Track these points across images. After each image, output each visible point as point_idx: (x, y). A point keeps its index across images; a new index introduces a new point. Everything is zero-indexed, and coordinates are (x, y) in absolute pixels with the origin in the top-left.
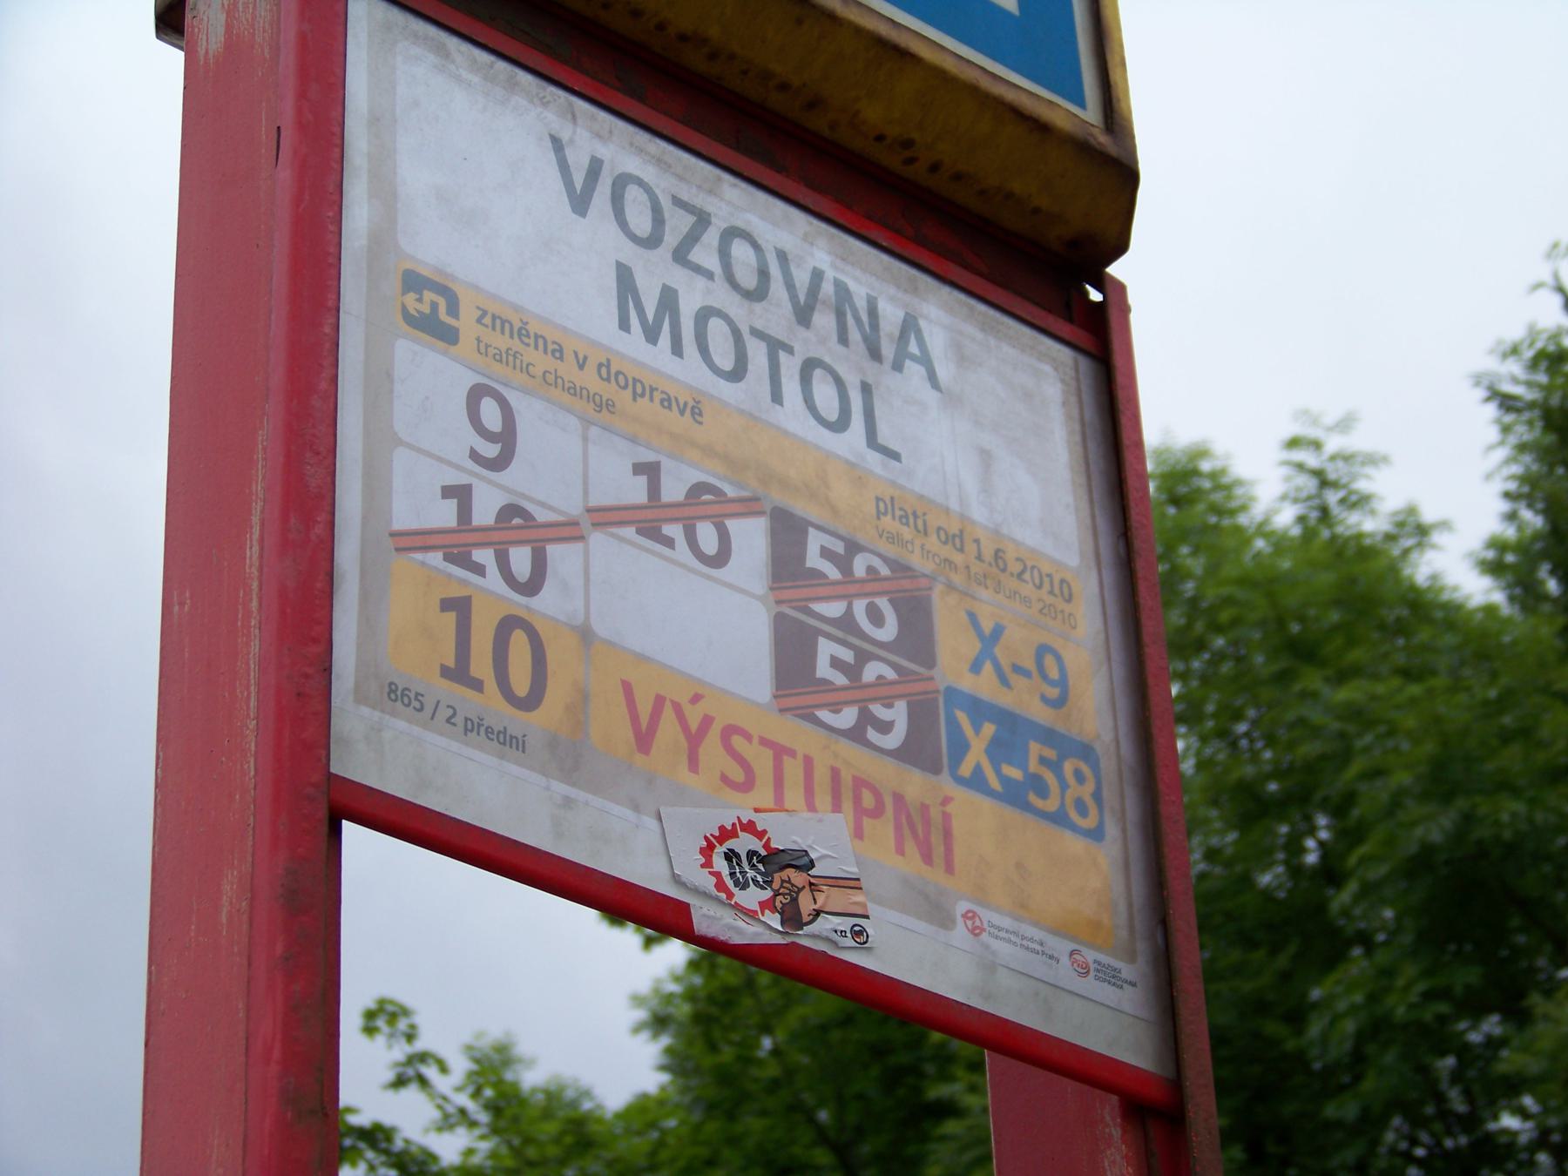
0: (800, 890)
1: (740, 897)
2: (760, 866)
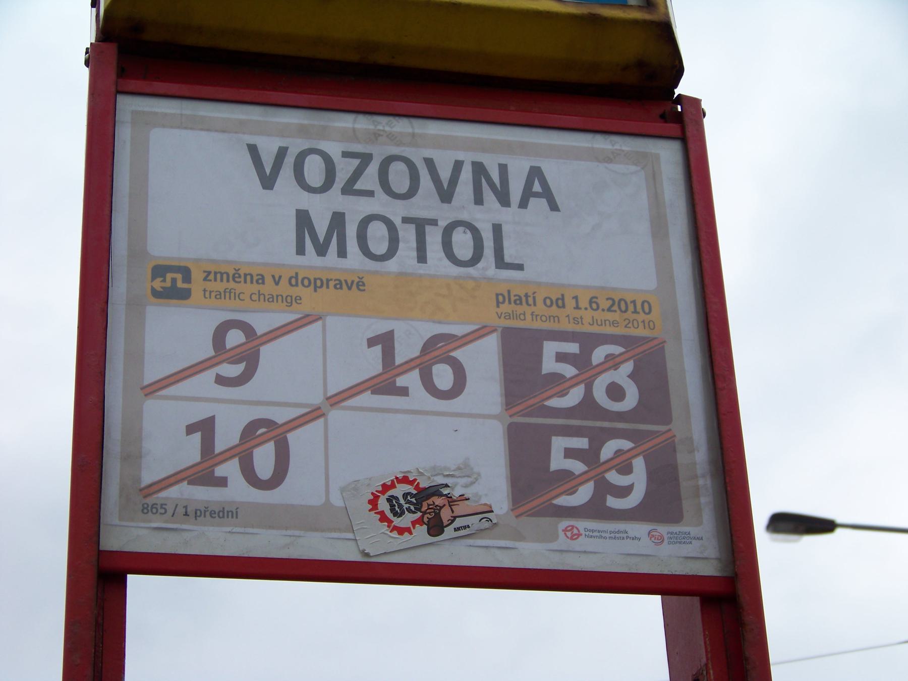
0: (441, 507)
1: (398, 522)
2: (413, 500)
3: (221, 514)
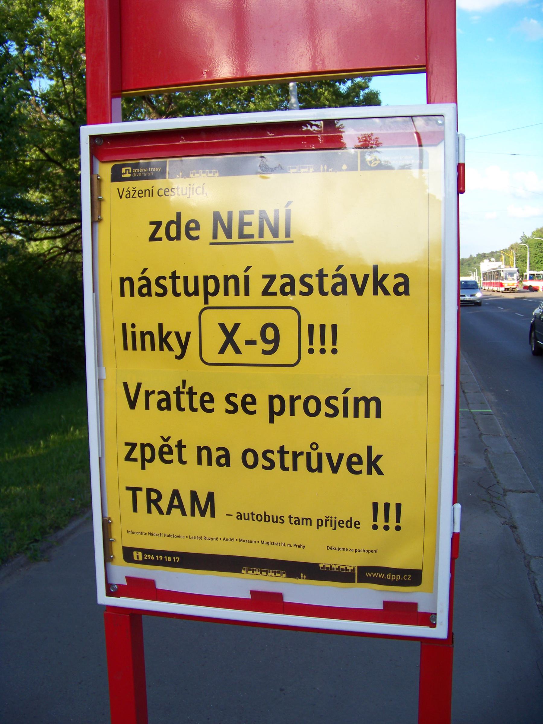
3: (349, 524)
